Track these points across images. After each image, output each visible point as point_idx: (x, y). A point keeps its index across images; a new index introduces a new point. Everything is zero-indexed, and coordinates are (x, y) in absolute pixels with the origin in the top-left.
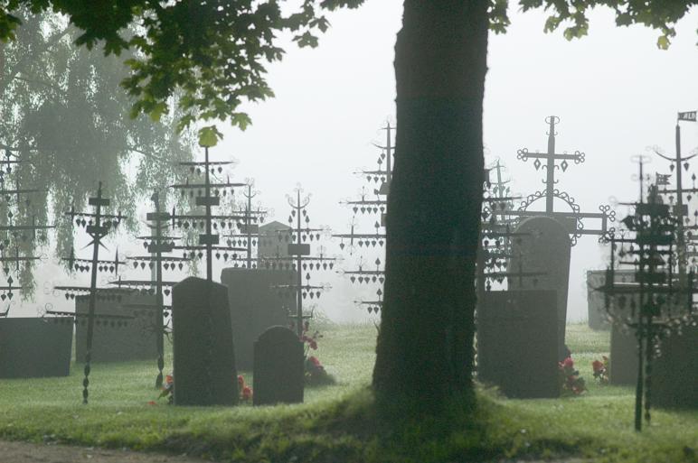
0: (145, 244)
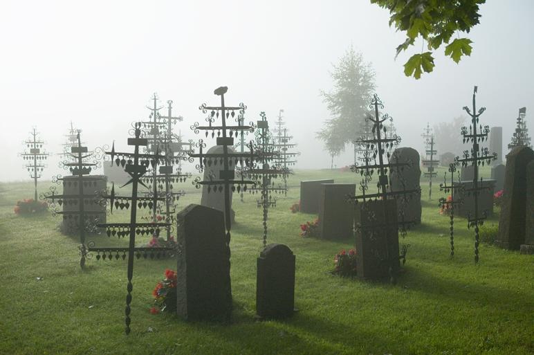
0: (71, 169)
